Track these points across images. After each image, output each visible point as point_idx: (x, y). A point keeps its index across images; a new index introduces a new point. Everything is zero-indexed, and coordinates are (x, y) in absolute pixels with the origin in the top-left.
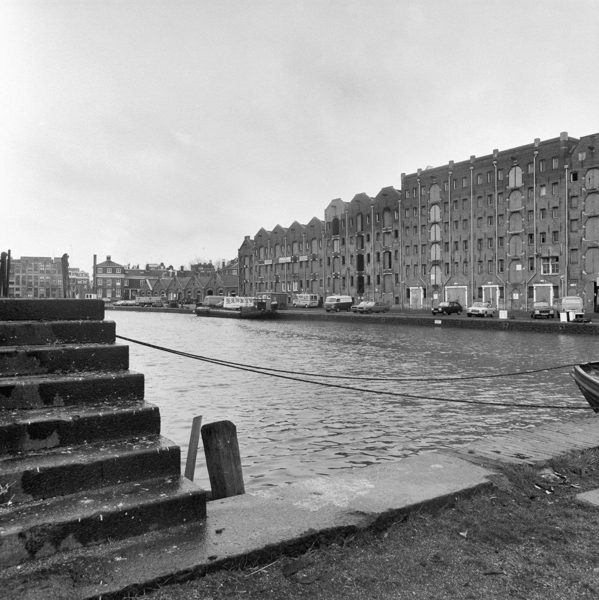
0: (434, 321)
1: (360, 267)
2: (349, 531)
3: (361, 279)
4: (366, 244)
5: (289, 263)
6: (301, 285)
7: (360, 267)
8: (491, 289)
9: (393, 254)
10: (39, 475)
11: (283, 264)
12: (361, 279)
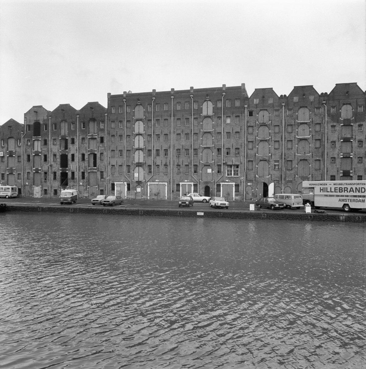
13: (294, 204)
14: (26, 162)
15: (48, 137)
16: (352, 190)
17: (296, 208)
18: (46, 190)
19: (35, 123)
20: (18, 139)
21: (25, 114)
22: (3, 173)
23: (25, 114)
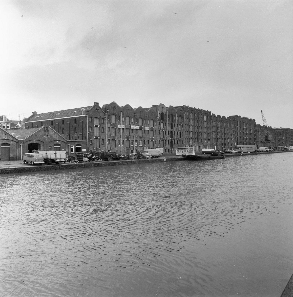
0: (164, 160)
1: (172, 137)
2: (208, 154)
3: (172, 141)
4: (174, 127)
5: (137, 130)
6: (144, 143)
7: (172, 137)
8: (3, 120)
9: (182, 133)
10: (187, 160)
11: (132, 129)
12: (172, 141)
13: (35, 161)
14: (158, 134)
15: (167, 122)
16: (250, 147)
17: (39, 164)
18: (165, 150)
19: (161, 113)
20: (154, 121)
21: (254, 120)
22: (149, 140)
23: (254, 120)
